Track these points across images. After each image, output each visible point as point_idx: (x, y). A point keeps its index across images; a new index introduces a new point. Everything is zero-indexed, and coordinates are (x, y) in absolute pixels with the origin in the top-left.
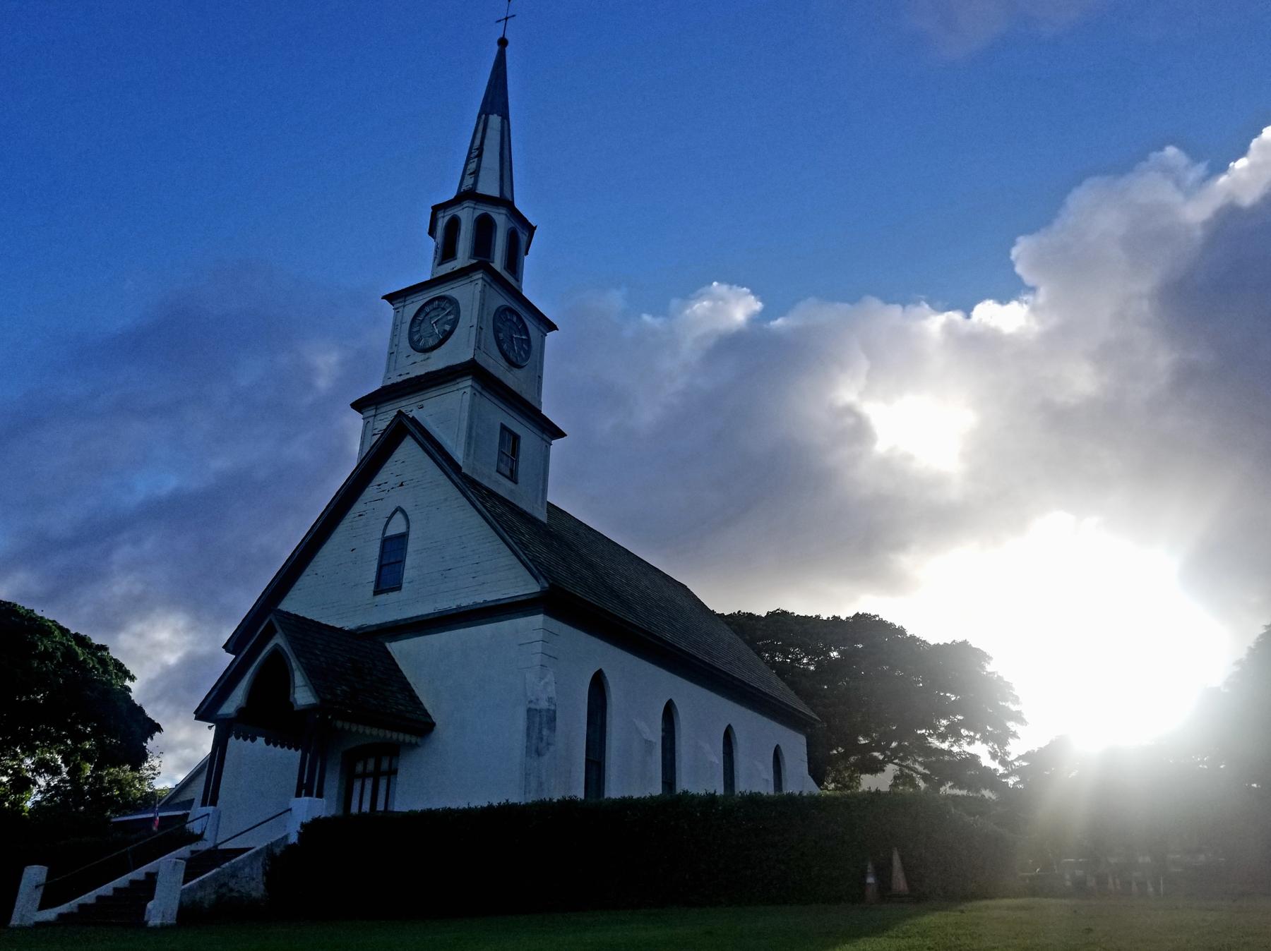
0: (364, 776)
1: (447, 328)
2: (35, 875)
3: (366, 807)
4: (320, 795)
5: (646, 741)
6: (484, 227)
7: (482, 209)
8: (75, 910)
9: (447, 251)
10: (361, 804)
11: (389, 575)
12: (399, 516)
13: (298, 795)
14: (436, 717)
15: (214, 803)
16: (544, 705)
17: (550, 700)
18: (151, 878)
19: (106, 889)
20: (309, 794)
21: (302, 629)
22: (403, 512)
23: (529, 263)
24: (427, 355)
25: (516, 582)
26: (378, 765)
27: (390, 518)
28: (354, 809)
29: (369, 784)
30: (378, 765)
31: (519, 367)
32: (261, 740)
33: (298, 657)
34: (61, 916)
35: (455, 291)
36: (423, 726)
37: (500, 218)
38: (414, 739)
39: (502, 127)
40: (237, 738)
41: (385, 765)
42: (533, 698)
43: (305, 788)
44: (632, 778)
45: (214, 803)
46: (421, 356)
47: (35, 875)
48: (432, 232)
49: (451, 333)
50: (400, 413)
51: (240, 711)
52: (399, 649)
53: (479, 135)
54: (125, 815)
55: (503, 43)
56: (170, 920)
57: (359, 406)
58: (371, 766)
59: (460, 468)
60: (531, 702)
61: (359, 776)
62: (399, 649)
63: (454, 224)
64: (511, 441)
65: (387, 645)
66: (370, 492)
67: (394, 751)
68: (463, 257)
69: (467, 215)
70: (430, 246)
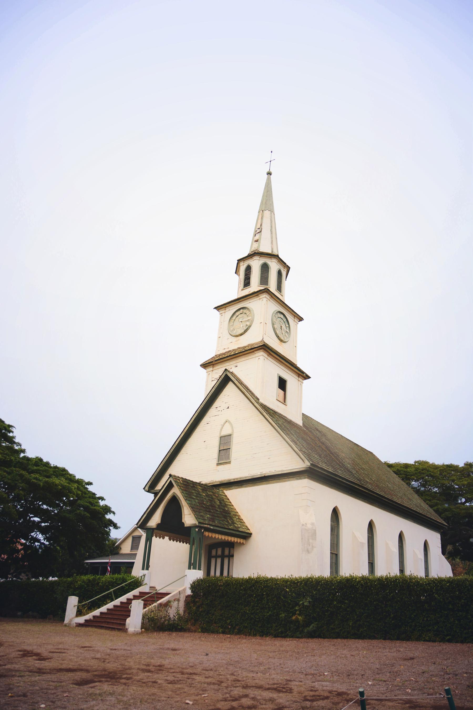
0: (216, 557)
1: (248, 323)
2: (73, 601)
3: (218, 574)
4: (199, 569)
5: (361, 542)
6: (265, 268)
7: (263, 260)
8: (92, 618)
9: (247, 283)
10: (216, 572)
11: (224, 454)
12: (227, 424)
13: (189, 568)
14: (252, 531)
15: (147, 569)
16: (309, 526)
17: (313, 524)
18: (79, 613)
19: (104, 609)
20: (194, 568)
21: (188, 486)
22: (229, 422)
23: (286, 284)
24: (238, 338)
25: (286, 458)
26: (223, 552)
27: (223, 425)
28: (212, 573)
29: (219, 561)
30: (223, 552)
31: (285, 342)
32: (167, 538)
33: (186, 500)
34: (86, 621)
35: (252, 304)
36: (247, 536)
37: (274, 266)
38: (242, 541)
39: (271, 217)
40: (156, 537)
41: (227, 552)
42: (304, 523)
43: (192, 565)
44: (353, 566)
45: (147, 569)
46: (235, 339)
47: (73, 601)
48: (237, 272)
49: (250, 327)
50: (226, 370)
51: (158, 525)
52: (232, 495)
53: (259, 221)
54: (94, 558)
55: (269, 174)
56: (138, 629)
57: (205, 366)
58: (219, 552)
59: (258, 399)
60: (303, 525)
61: (213, 557)
62: (232, 495)
63: (248, 269)
64: (282, 384)
65: (225, 491)
66: (212, 411)
67: (231, 545)
68: (255, 285)
69: (256, 264)
70: (238, 280)
